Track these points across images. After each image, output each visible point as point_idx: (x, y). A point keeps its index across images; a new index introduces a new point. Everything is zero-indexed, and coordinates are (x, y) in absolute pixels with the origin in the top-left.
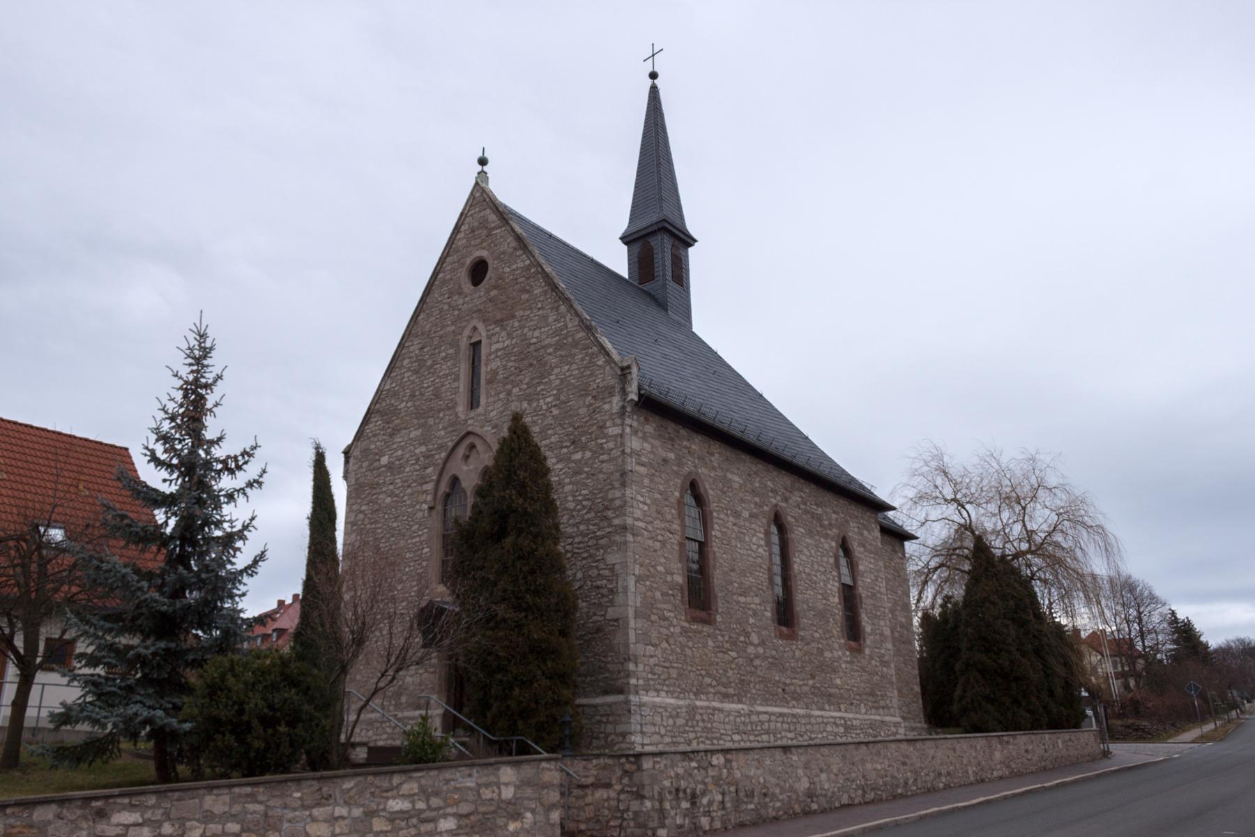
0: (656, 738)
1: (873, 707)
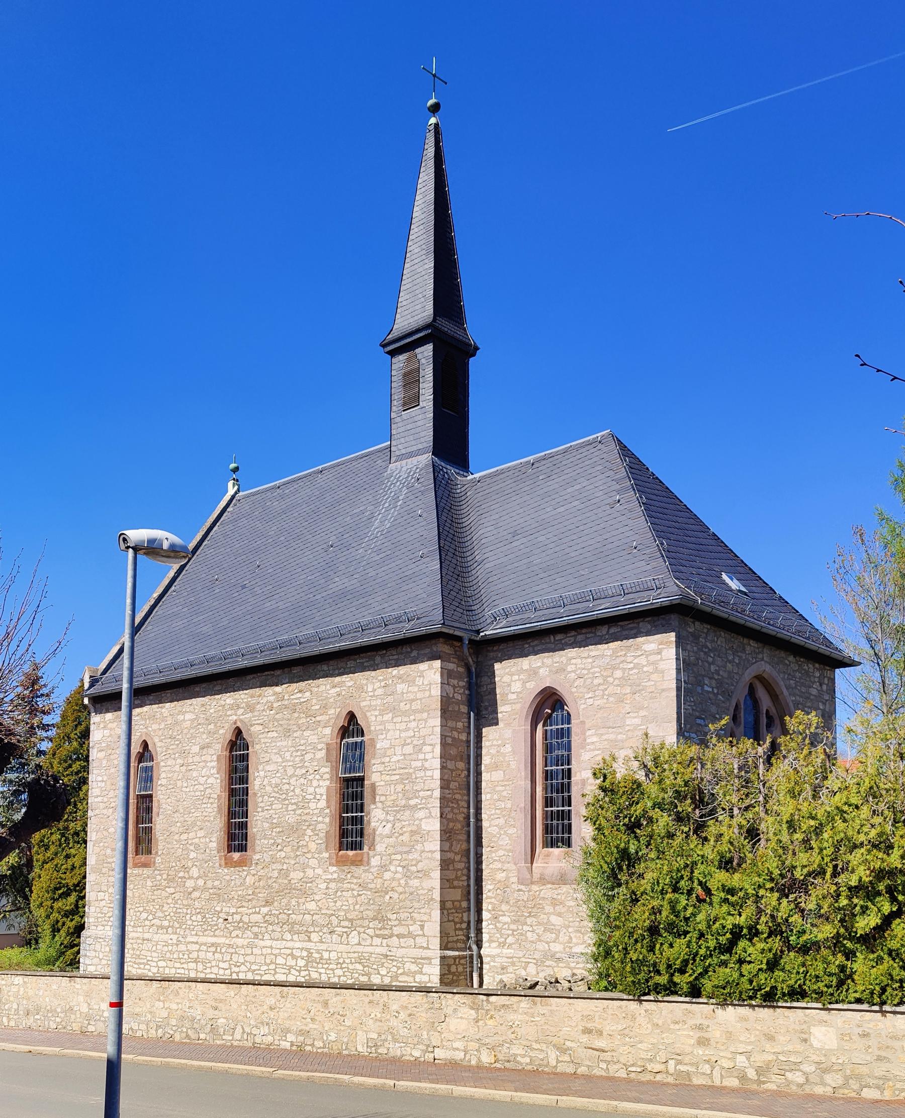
0: (96, 961)
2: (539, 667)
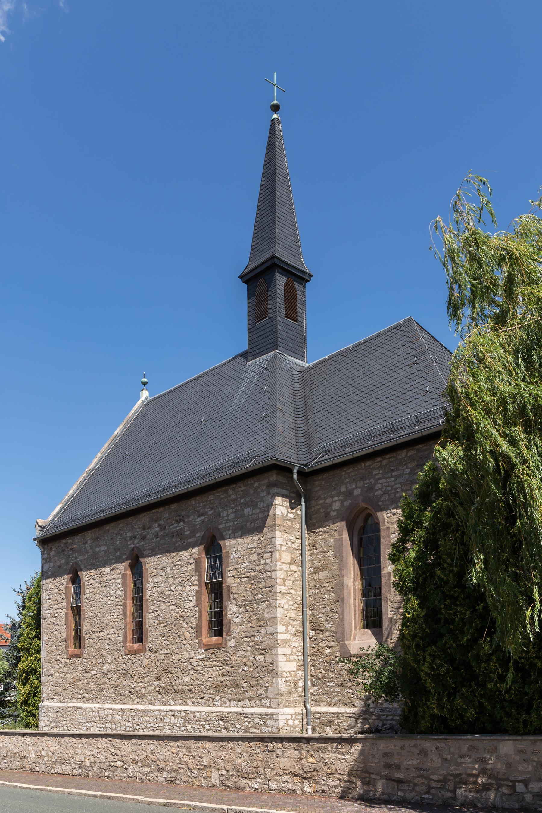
1: (234, 700)
2: (354, 489)
